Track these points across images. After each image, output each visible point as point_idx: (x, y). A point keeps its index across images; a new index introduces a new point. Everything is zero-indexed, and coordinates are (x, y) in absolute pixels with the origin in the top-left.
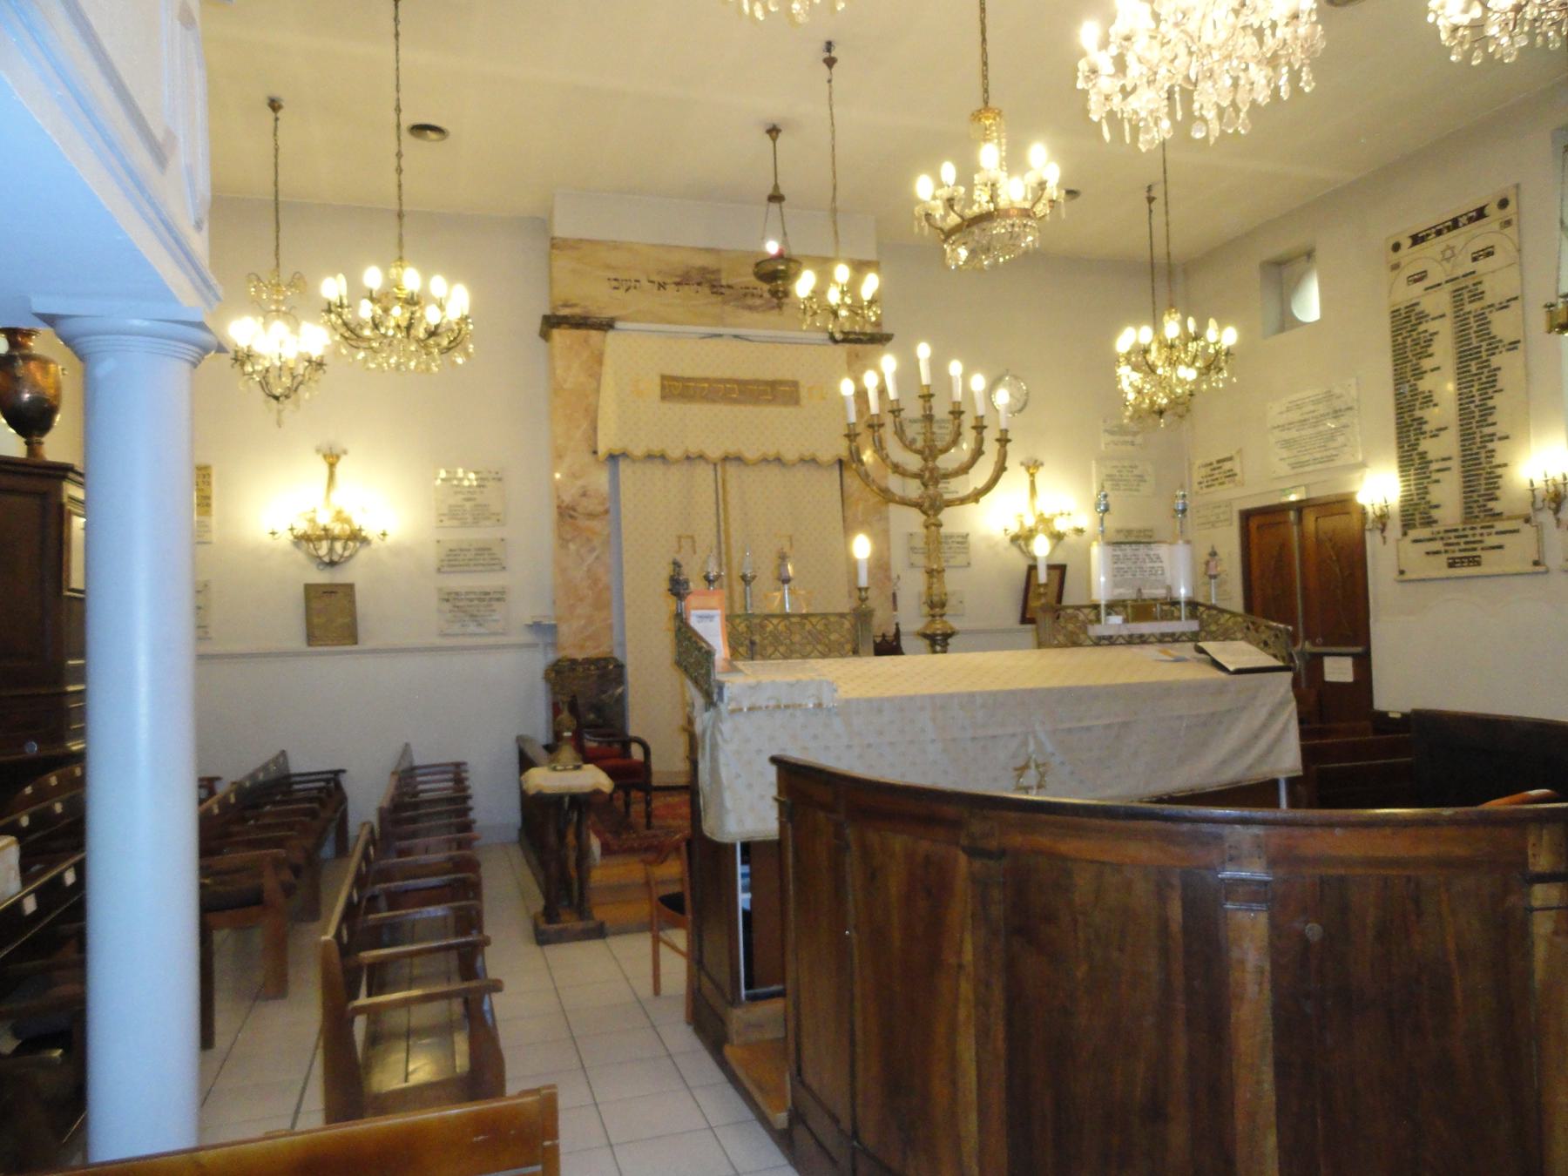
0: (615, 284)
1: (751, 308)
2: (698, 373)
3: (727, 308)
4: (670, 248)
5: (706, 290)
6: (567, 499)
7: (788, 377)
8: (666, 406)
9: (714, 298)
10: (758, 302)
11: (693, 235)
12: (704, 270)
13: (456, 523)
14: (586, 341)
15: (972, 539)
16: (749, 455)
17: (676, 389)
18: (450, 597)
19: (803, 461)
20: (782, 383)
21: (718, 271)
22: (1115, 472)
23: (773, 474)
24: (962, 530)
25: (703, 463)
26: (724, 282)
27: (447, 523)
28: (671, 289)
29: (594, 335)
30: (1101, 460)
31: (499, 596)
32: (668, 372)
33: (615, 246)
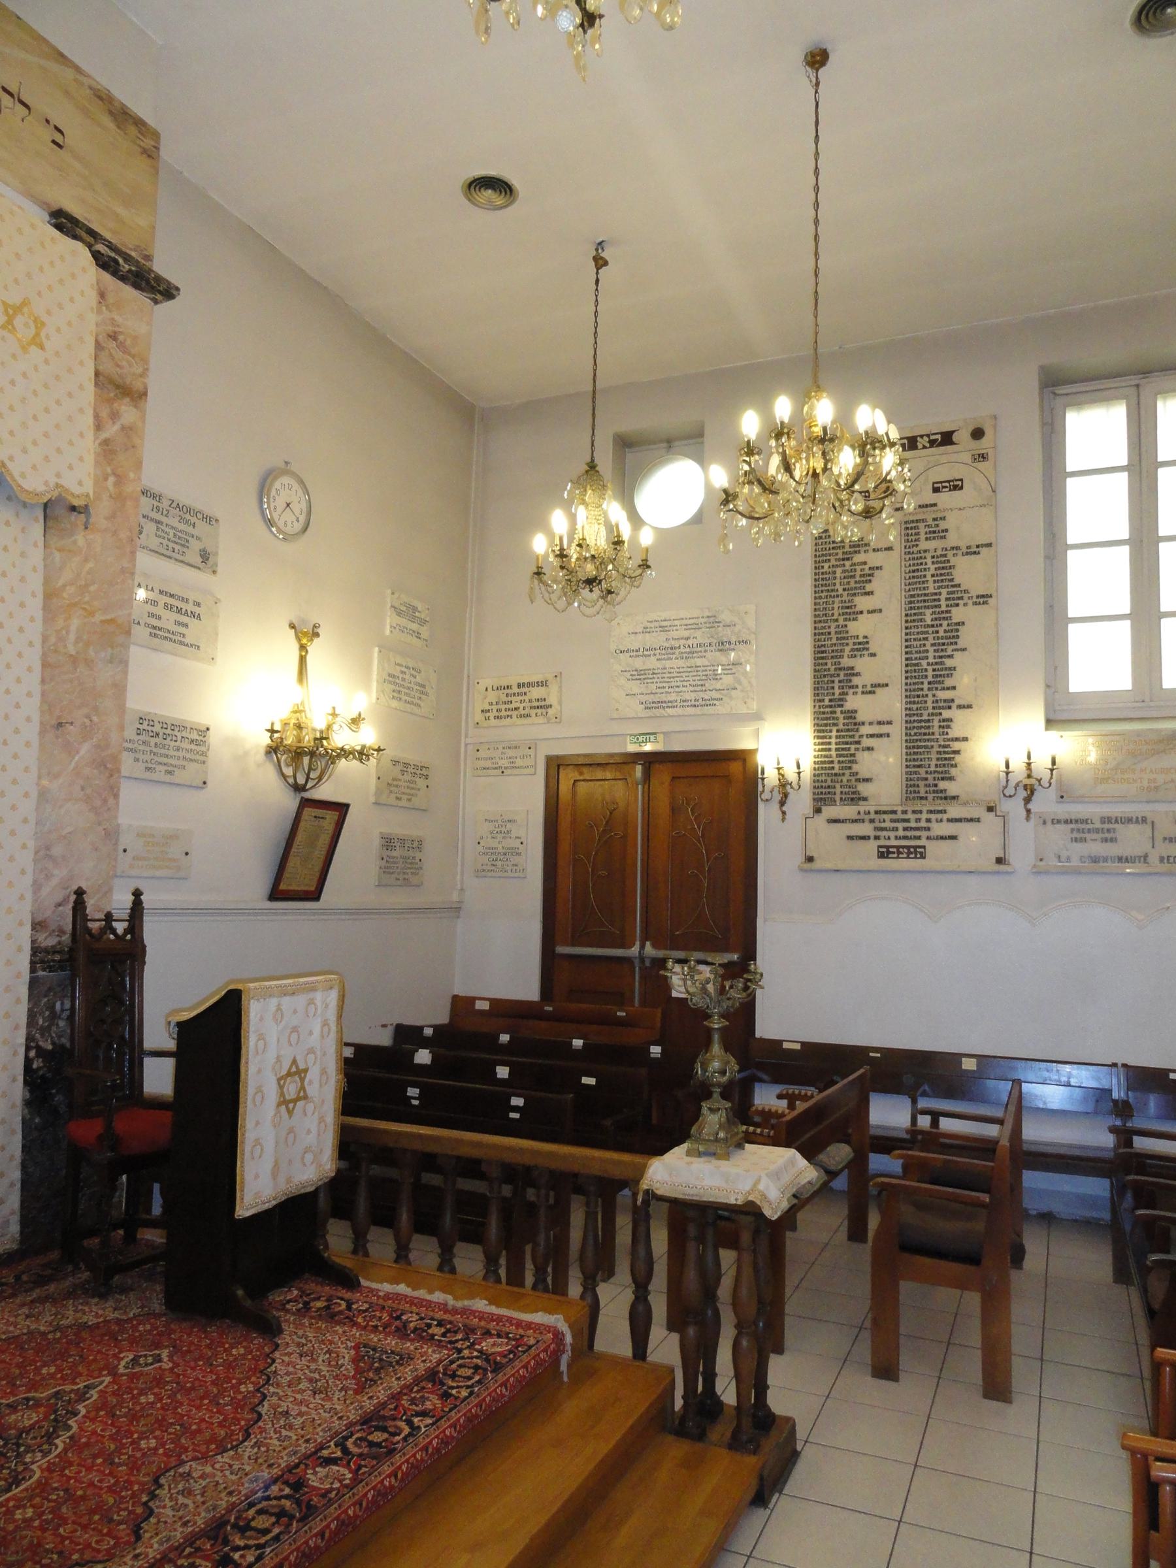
15: (213, 738)
22: (397, 671)
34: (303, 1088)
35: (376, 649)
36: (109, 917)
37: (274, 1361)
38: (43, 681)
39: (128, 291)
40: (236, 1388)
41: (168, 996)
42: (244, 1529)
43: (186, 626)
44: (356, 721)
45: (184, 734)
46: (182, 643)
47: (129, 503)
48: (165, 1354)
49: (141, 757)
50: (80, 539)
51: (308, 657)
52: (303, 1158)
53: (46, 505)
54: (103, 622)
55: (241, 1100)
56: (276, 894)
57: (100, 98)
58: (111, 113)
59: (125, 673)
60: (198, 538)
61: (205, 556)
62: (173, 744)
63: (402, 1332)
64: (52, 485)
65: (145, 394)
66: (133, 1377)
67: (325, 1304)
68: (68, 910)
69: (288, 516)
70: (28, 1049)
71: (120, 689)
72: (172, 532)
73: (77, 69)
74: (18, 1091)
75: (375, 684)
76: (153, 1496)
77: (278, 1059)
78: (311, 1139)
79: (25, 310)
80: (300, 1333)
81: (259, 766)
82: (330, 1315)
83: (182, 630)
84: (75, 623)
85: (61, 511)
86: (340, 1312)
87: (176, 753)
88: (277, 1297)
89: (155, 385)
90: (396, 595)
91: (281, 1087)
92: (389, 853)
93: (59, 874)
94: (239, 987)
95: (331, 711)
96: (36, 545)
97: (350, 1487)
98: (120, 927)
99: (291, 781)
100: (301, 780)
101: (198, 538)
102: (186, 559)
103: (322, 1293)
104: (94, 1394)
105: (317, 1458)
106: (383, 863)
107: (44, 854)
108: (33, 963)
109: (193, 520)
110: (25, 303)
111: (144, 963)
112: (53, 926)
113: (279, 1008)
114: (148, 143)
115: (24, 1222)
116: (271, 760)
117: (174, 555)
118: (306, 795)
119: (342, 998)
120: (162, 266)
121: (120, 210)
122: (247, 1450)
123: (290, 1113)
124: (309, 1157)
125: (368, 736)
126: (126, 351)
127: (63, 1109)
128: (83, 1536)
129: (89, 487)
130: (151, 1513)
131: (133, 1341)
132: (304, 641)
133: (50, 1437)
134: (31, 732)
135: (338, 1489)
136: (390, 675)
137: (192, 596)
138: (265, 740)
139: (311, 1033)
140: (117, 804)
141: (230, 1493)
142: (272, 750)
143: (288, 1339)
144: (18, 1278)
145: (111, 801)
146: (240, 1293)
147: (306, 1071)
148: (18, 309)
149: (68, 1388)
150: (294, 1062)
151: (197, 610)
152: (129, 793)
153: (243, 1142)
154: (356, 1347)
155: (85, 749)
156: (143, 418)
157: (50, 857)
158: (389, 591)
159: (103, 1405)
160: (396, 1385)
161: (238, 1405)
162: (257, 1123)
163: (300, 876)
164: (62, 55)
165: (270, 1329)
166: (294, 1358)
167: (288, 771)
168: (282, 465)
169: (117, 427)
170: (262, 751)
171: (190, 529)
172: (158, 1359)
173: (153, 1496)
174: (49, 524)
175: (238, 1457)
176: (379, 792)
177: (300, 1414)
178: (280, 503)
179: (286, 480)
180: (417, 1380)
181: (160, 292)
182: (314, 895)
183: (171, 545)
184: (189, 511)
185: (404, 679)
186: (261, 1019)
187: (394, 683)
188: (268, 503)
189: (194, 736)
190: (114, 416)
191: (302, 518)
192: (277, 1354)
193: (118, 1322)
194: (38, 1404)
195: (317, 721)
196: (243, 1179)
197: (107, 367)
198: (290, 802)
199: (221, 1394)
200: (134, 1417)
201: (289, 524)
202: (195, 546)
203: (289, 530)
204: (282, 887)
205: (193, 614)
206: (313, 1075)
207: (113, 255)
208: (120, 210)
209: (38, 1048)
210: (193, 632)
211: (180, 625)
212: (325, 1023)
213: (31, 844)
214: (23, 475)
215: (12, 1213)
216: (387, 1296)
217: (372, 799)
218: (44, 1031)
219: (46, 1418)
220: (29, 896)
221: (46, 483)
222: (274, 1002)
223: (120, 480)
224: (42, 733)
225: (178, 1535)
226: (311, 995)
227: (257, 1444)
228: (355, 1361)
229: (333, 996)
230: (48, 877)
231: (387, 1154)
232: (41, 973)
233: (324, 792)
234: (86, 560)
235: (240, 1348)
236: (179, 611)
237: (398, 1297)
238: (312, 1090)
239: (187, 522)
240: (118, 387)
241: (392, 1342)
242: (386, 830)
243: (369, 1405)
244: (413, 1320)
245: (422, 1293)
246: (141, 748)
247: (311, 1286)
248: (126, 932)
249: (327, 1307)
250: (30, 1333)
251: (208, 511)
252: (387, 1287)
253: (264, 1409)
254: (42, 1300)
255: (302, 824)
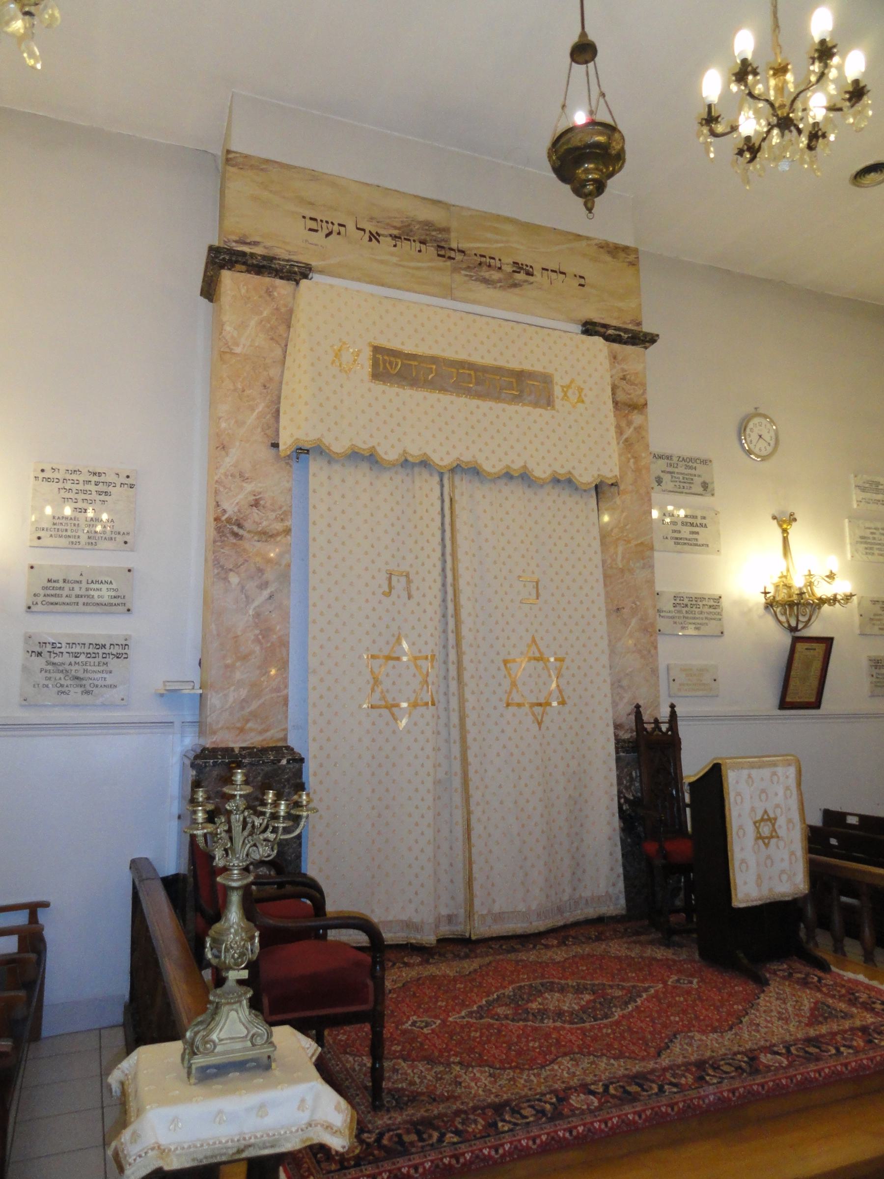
0: (313, 225)
1: (486, 281)
2: (422, 350)
3: (459, 278)
4: (387, 192)
5: (431, 250)
6: (230, 507)
7: (538, 368)
8: (379, 388)
9: (440, 263)
10: (496, 275)
11: (417, 182)
12: (428, 225)
13: (63, 542)
14: (269, 293)
15: (725, 603)
16: (490, 466)
17: (393, 367)
18: (39, 649)
19: (556, 481)
20: (531, 375)
21: (447, 230)
22: (867, 533)
23: (514, 497)
24: (715, 591)
25: (425, 474)
26: (454, 245)
27: (47, 541)
28: (387, 242)
29: (282, 287)
30: (854, 518)
31: (120, 651)
32: (383, 342)
33: (314, 176)
34: (774, 830)
35: (847, 520)
36: (656, 722)
37: (759, 998)
38: (605, 585)
39: (629, 348)
40: (732, 1006)
41: (692, 767)
42: (716, 1068)
43: (697, 533)
44: (831, 576)
45: (704, 603)
46: (696, 545)
47: (644, 472)
48: (695, 981)
49: (677, 620)
50: (618, 500)
51: (790, 537)
52: (780, 877)
53: (596, 487)
54: (636, 545)
55: (729, 833)
56: (784, 704)
57: (602, 247)
58: (609, 252)
59: (653, 573)
60: (699, 476)
61: (705, 486)
62: (697, 610)
63: (853, 1002)
64: (596, 476)
65: (646, 404)
66: (674, 987)
67: (803, 976)
68: (633, 717)
69: (762, 444)
70: (619, 798)
71: (651, 582)
72: (681, 477)
73: (588, 238)
74: (616, 822)
75: (848, 547)
76: (671, 1041)
77: (753, 809)
78: (785, 865)
79: (573, 385)
80: (781, 987)
81: (760, 617)
82: (805, 983)
83: (695, 536)
84: (620, 550)
85: (606, 488)
86: (812, 983)
87: (701, 616)
88: (774, 966)
89: (653, 397)
90: (859, 476)
91: (757, 828)
92: (877, 671)
93: (627, 696)
94: (720, 762)
95: (807, 573)
96: (593, 510)
97: (784, 1068)
98: (664, 727)
99: (786, 625)
100: (793, 623)
101: (699, 476)
102: (693, 491)
103: (802, 969)
104: (652, 991)
105: (770, 1049)
106: (874, 679)
107: (617, 685)
108: (617, 749)
109: (694, 465)
110: (572, 381)
111: (681, 749)
112: (627, 727)
113: (750, 776)
114: (632, 258)
115: (628, 899)
116: (769, 612)
117: (685, 491)
118: (798, 634)
119: (799, 773)
120: (647, 328)
121: (620, 304)
122: (729, 1035)
123: (767, 845)
124: (784, 877)
125: (843, 586)
126: (632, 384)
127: (643, 835)
128: (632, 1047)
129: (617, 472)
130: (668, 1047)
131: (679, 971)
132: (785, 526)
133: (626, 1004)
134: (602, 616)
135: (776, 1067)
136: (862, 537)
137: (699, 514)
138: (762, 600)
139: (776, 794)
140: (657, 653)
141: (713, 1052)
142: (770, 605)
143: (772, 989)
144: (626, 930)
145: (653, 651)
146: (742, 955)
147: (775, 819)
148: (569, 387)
149: (639, 984)
150: (766, 812)
151: (704, 521)
152: (665, 646)
153: (733, 859)
154: (816, 1003)
155: (634, 622)
156: (646, 420)
157: (621, 687)
158: (852, 475)
159: (656, 995)
160: (835, 1028)
161: (729, 1014)
162: (742, 849)
163: (802, 691)
164: (579, 235)
165: (762, 983)
166: (773, 999)
167: (783, 619)
168: (753, 411)
169: (632, 429)
170: (762, 607)
171: (693, 472)
172: (691, 983)
173: (671, 1041)
174: (600, 496)
175: (722, 1037)
176: (862, 626)
177: (766, 1027)
178: (754, 437)
179: (756, 420)
180: (852, 1029)
181: (648, 342)
182: (817, 705)
183: (682, 485)
184: (691, 460)
185: (874, 538)
186: (737, 782)
187: (866, 543)
188: (745, 439)
189: (712, 603)
190: (629, 423)
191: (772, 443)
192: (762, 995)
193: (674, 961)
194: (623, 988)
195: (798, 582)
196: (735, 885)
197: (621, 396)
198: (786, 639)
199: (722, 1006)
200: (670, 1005)
201: (763, 449)
202: (698, 481)
203: (764, 453)
204: (788, 699)
205: (701, 525)
206: (781, 822)
207: (618, 333)
208: (620, 304)
209: (625, 797)
210: (703, 535)
211: (692, 536)
212: (787, 788)
213: (608, 680)
214: (581, 475)
215: (620, 892)
216: (850, 980)
217: (858, 632)
218: (628, 788)
219: (626, 994)
220: (610, 709)
221: (593, 476)
222: (745, 772)
223: (636, 458)
224: (608, 615)
225: (680, 1060)
226: (775, 769)
227: (736, 1034)
228: (812, 1010)
229: (792, 771)
230: (621, 698)
231: (850, 887)
232: (622, 754)
233: (816, 629)
234: (623, 512)
235: (741, 987)
236: (692, 525)
237: (857, 983)
238: (782, 832)
239: (691, 468)
240: (629, 406)
241: (843, 1006)
242: (873, 654)
243: (812, 1033)
244: (863, 997)
245: (875, 983)
246: (677, 615)
247: (798, 966)
248: (668, 730)
249: (804, 979)
250: (627, 956)
251: (703, 457)
252: (850, 975)
253: (744, 1020)
254: (635, 942)
255: (797, 655)
